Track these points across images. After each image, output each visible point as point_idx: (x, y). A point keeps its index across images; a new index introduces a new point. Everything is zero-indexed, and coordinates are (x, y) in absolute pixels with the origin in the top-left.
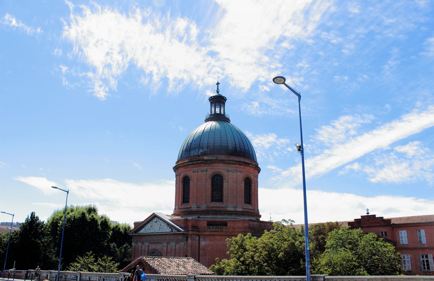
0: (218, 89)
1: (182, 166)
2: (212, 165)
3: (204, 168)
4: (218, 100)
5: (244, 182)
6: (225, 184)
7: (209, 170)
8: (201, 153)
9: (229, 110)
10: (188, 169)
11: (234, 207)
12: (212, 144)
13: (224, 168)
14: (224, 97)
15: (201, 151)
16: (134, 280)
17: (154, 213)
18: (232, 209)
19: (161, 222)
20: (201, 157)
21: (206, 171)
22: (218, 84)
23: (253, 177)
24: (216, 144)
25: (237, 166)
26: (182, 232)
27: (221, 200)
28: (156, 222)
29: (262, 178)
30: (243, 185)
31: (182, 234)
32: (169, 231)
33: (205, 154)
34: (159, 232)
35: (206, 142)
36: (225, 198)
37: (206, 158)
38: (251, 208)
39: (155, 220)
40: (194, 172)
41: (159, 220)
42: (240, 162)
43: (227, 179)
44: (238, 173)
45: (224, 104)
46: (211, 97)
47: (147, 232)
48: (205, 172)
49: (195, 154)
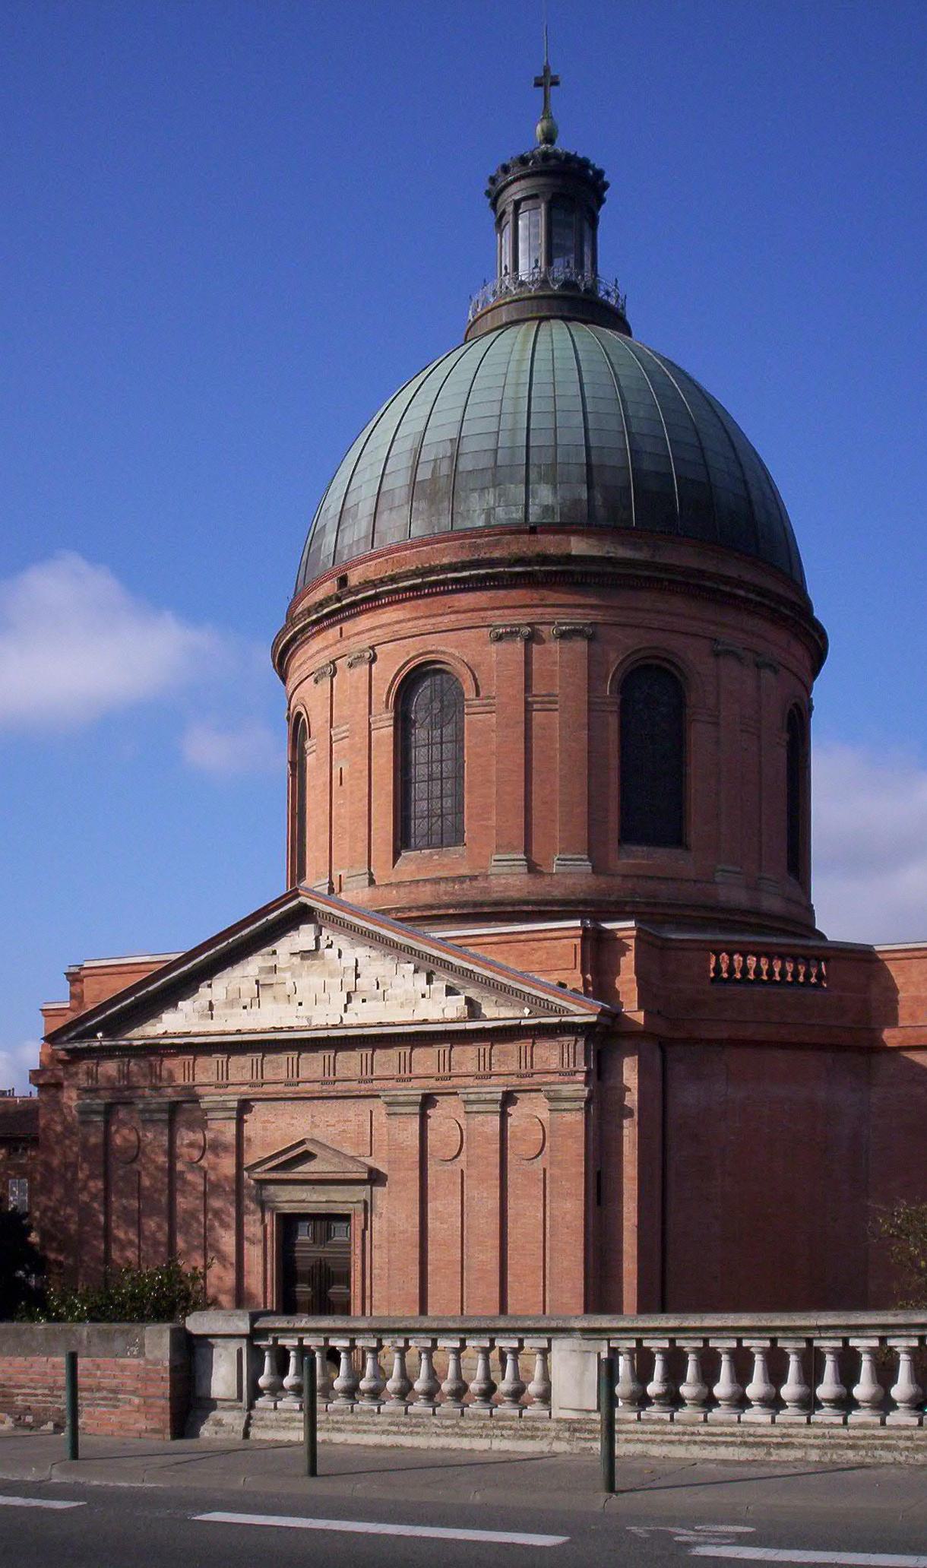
6: (699, 737)
8: (547, 509)
10: (447, 621)
15: (544, 495)
18: (480, 523)
19: (362, 952)
21: (776, 672)
27: (674, 836)
28: (305, 955)
32: (451, 1014)
35: (572, 435)
36: (696, 828)
37: (578, 546)
39: (303, 937)
40: (499, 638)
41: (341, 941)
49: (501, 515)
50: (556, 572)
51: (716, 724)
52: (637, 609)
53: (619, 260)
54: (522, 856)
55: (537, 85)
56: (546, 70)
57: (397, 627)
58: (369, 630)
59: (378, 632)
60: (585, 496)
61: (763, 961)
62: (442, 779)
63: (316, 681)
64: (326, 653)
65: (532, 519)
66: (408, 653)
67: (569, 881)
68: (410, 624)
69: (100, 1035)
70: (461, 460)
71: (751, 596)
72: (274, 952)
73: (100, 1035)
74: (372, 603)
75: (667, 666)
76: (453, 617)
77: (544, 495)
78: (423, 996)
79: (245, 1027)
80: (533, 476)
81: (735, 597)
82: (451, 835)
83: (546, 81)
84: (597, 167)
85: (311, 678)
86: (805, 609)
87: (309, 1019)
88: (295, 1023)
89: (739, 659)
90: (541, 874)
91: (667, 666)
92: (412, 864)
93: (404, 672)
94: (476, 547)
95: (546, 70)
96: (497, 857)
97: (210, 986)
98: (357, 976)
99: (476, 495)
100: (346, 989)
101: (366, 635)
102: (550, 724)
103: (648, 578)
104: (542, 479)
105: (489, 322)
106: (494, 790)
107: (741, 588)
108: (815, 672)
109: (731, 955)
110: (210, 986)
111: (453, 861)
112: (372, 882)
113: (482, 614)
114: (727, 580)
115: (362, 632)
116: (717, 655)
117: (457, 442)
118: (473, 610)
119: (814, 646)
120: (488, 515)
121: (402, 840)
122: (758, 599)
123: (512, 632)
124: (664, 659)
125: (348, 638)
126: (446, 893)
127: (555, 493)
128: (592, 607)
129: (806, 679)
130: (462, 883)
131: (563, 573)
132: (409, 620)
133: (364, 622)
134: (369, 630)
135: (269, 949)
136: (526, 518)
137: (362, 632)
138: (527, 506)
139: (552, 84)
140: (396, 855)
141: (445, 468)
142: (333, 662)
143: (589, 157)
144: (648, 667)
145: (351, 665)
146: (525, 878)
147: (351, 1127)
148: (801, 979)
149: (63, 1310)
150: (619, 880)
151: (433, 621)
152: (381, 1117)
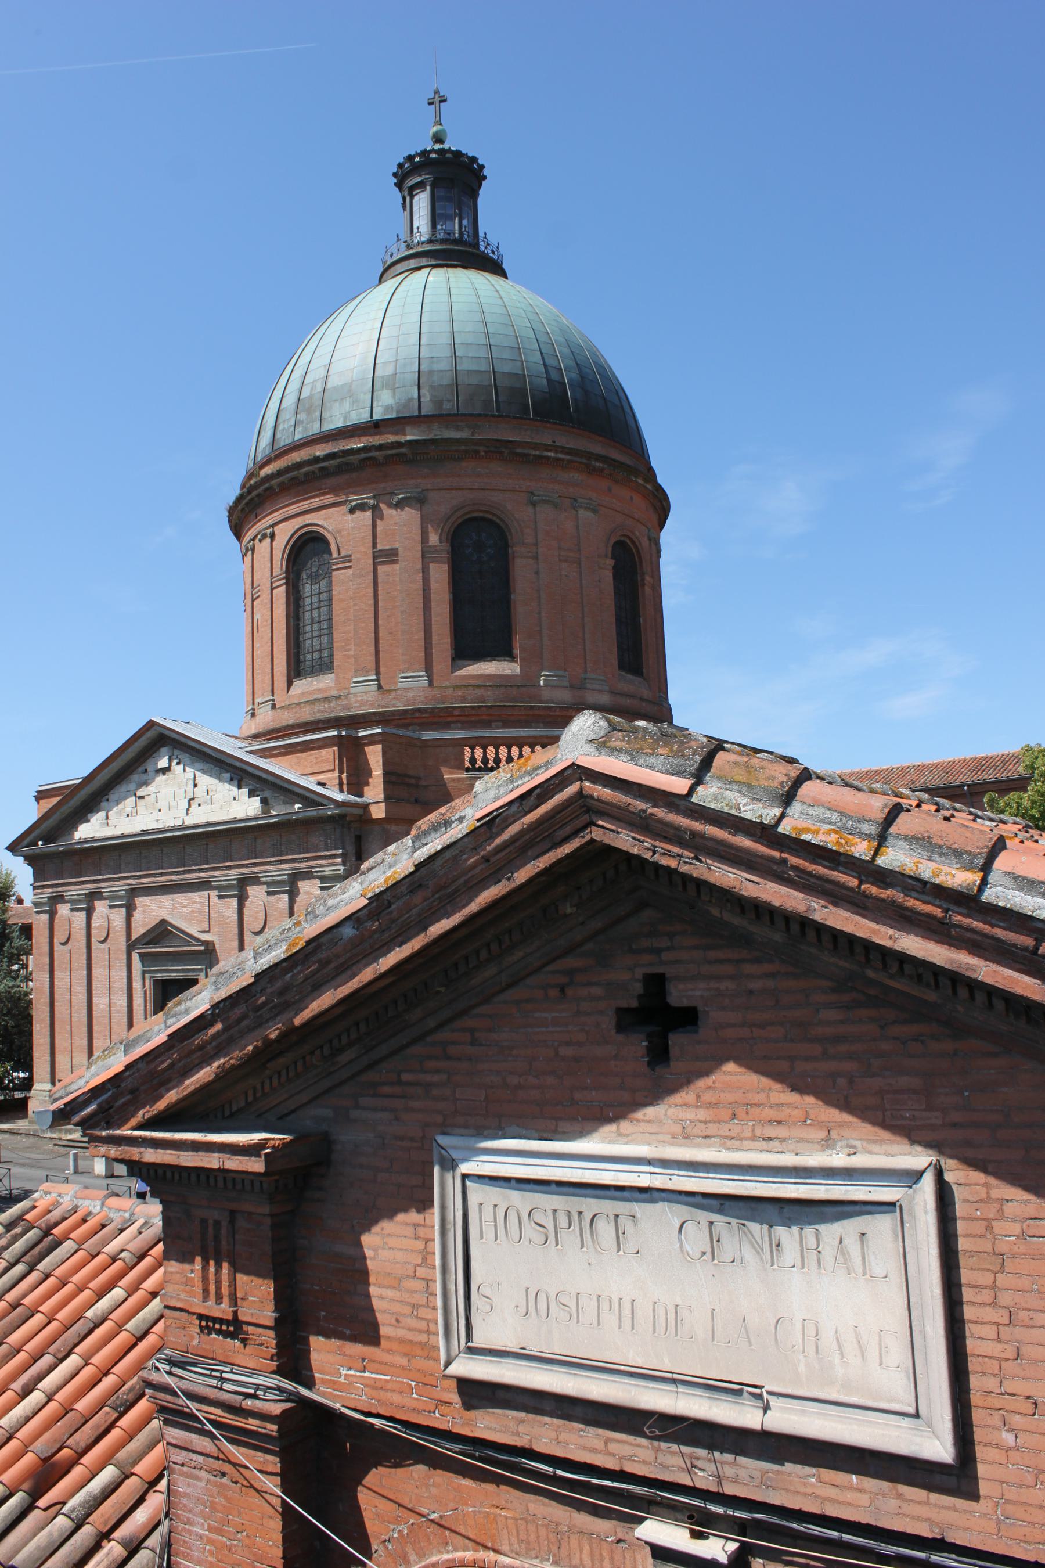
5: (610, 562)
6: (522, 570)
8: (387, 408)
10: (316, 502)
11: (572, 687)
12: (445, 365)
14: (474, 160)
16: (1038, 1516)
17: (151, 724)
22: (438, 100)
23: (645, 543)
24: (464, 366)
25: (576, 476)
26: (330, 811)
29: (680, 557)
30: (608, 575)
31: (331, 819)
34: (190, 821)
38: (646, 693)
40: (352, 511)
42: (590, 456)
43: (530, 540)
44: (582, 513)
45: (474, 194)
46: (410, 158)
47: (118, 832)
50: (392, 455)
51: (536, 558)
53: (495, 216)
54: (374, 677)
55: (430, 104)
56: (437, 92)
60: (416, 395)
61: (491, 750)
65: (375, 417)
67: (410, 694)
69: (40, 843)
71: (560, 456)
72: (146, 771)
73: (40, 843)
78: (235, 799)
79: (127, 832)
81: (548, 458)
82: (325, 666)
83: (438, 100)
84: (480, 162)
87: (604, 834)
88: (155, 826)
89: (556, 506)
90: (388, 691)
92: (301, 686)
93: (291, 543)
95: (437, 92)
96: (355, 680)
97: (108, 800)
98: (195, 786)
99: (337, 404)
100: (188, 797)
103: (466, 452)
105: (399, 268)
106: (352, 627)
107: (550, 451)
109: (497, 748)
110: (108, 800)
111: (323, 683)
112: (274, 706)
114: (536, 446)
116: (534, 504)
120: (345, 419)
121: (296, 670)
122: (568, 457)
123: (361, 504)
124: (487, 512)
126: (319, 711)
130: (330, 702)
131: (397, 455)
135: (141, 769)
136: (372, 417)
139: (441, 102)
140: (290, 684)
141: (319, 388)
143: (459, 149)
144: (475, 519)
145: (260, 541)
146: (376, 693)
147: (196, 908)
148: (479, 764)
150: (450, 691)
152: (214, 899)
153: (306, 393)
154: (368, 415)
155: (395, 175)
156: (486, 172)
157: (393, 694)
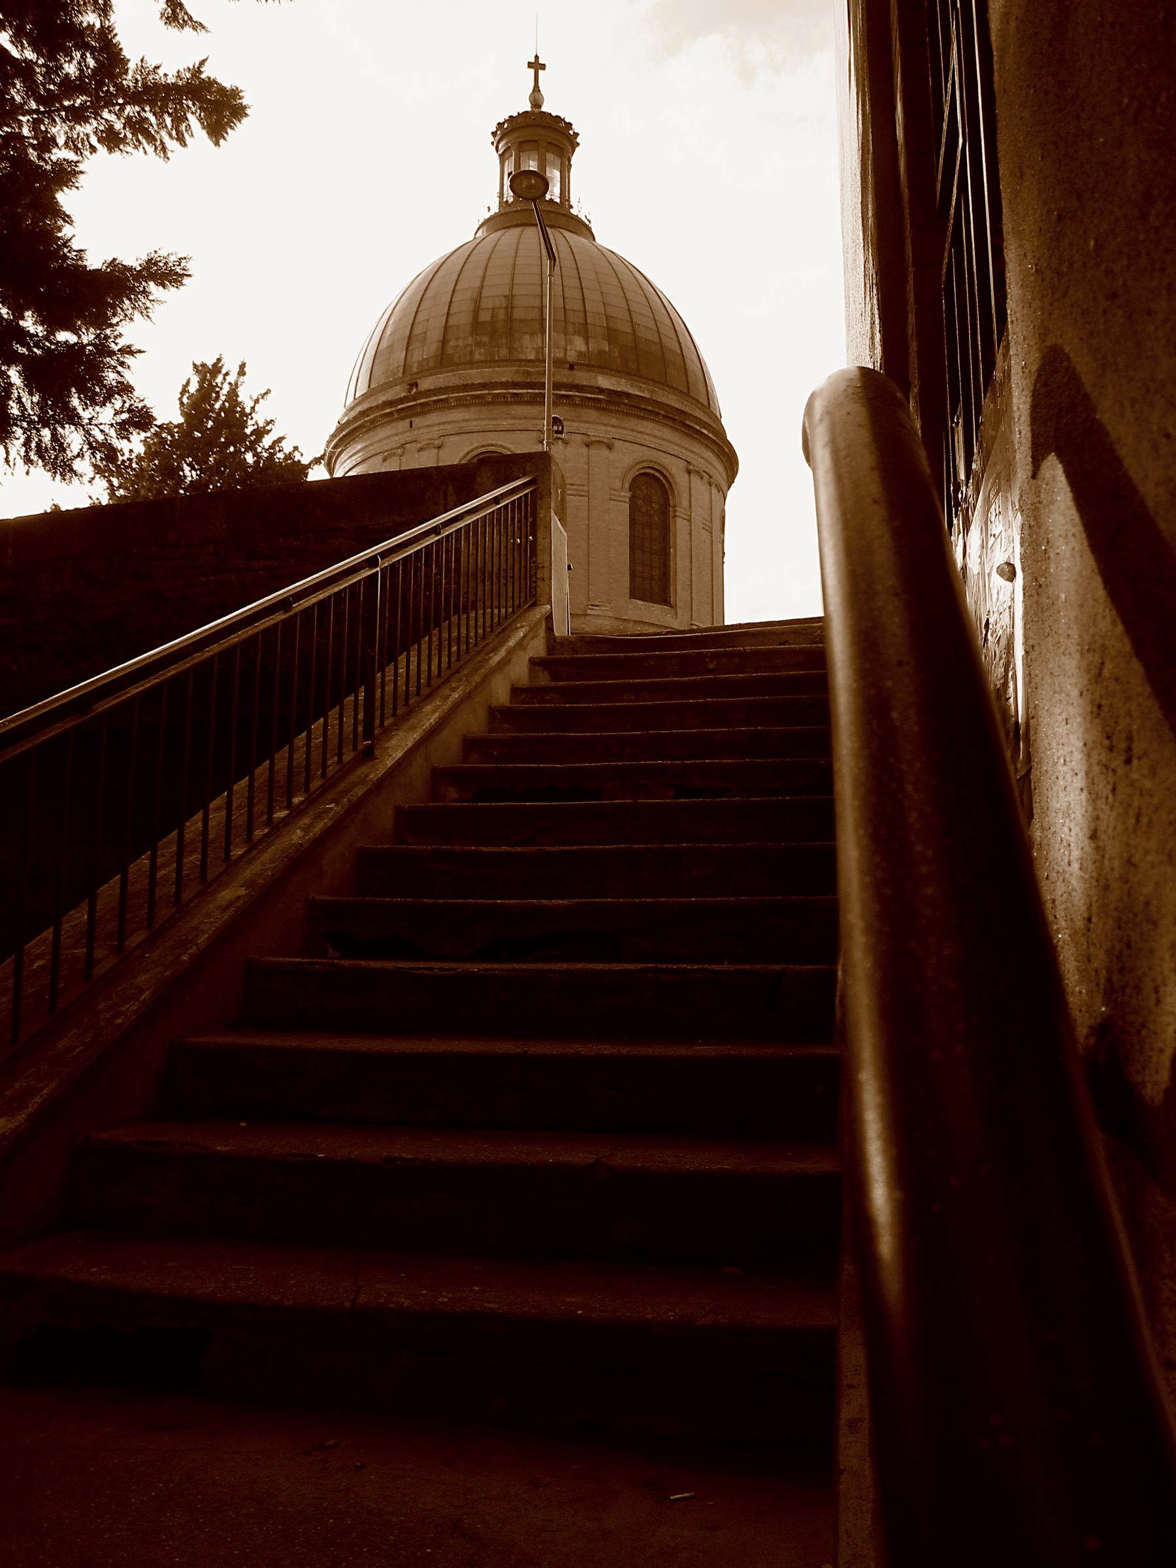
0: (536, 88)
1: (462, 404)
2: (633, 423)
3: (599, 431)
4: (538, 139)
7: (617, 443)
9: (592, 187)
13: (676, 450)
15: (579, 344)
20: (581, 377)
21: (610, 447)
33: (599, 364)
36: (680, 593)
48: (605, 452)
52: (656, 437)
56: (537, 57)
57: (464, 424)
58: (439, 424)
59: (447, 426)
62: (651, 554)
63: (385, 460)
64: (396, 438)
66: (472, 444)
68: (474, 423)
70: (515, 311)
74: (443, 405)
75: (657, 474)
76: (510, 421)
77: (579, 344)
80: (570, 328)
85: (380, 457)
86: (720, 433)
91: (657, 474)
94: (528, 373)
95: (537, 57)
101: (436, 428)
102: (826, 534)
104: (576, 333)
108: (731, 480)
113: (533, 422)
115: (432, 426)
116: (689, 472)
117: (510, 298)
118: (525, 418)
119: (729, 461)
120: (537, 353)
125: (419, 429)
127: (587, 343)
128: (987, 511)
129: (725, 488)
132: (475, 420)
133: (434, 418)
134: (439, 424)
137: (432, 426)
138: (566, 350)
141: (501, 315)
142: (402, 446)
149: (1097, 638)
151: (494, 422)
153: (485, 316)
154: (562, 355)
155: (494, 134)
156: (576, 128)
157: (582, 619)
